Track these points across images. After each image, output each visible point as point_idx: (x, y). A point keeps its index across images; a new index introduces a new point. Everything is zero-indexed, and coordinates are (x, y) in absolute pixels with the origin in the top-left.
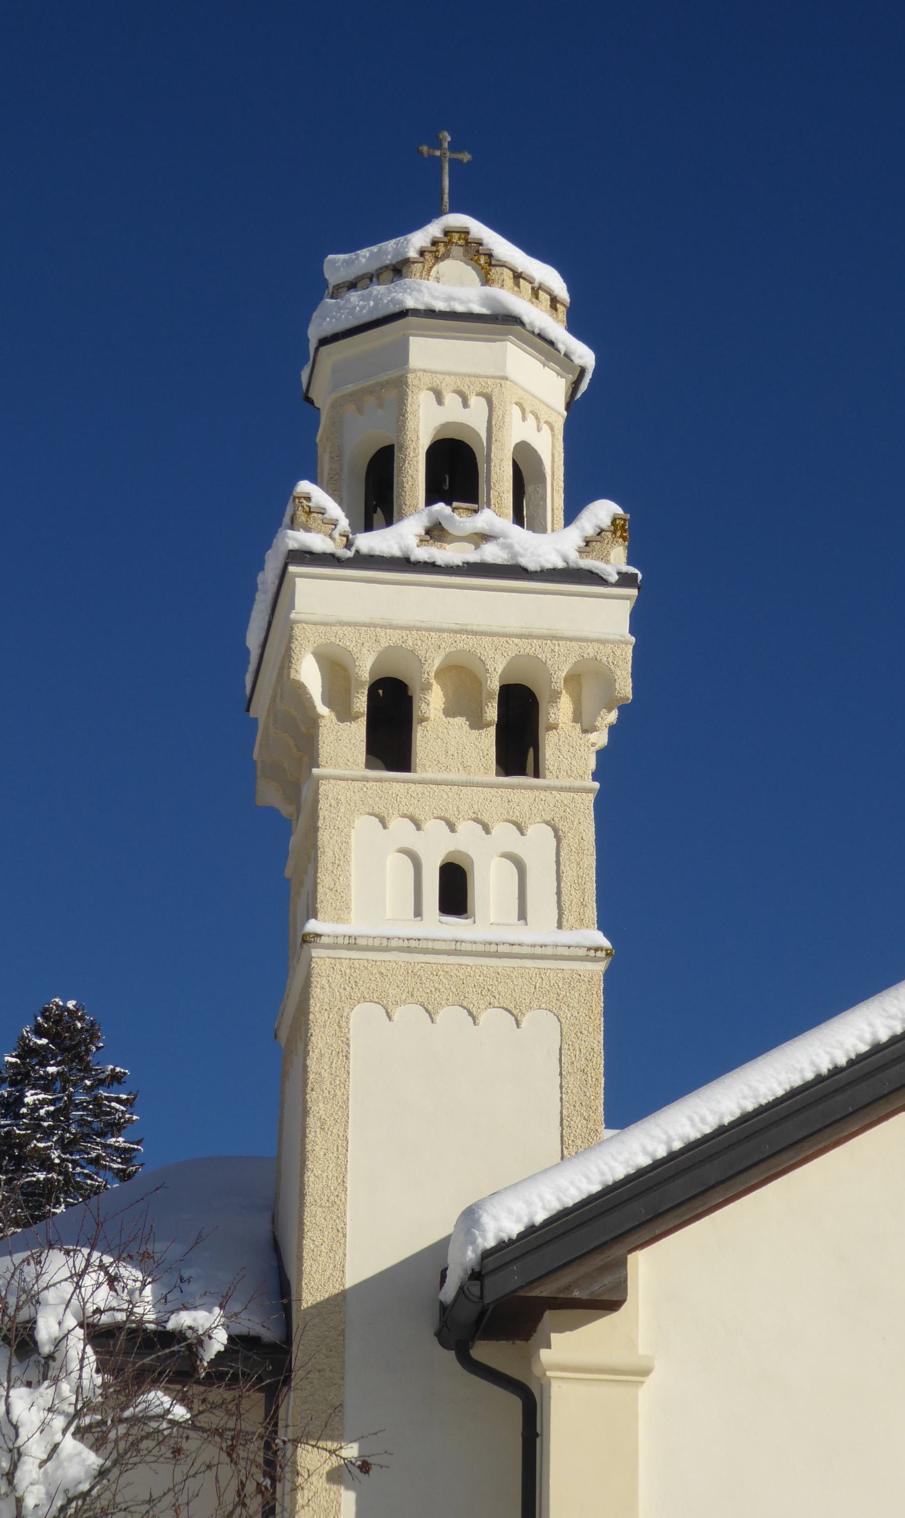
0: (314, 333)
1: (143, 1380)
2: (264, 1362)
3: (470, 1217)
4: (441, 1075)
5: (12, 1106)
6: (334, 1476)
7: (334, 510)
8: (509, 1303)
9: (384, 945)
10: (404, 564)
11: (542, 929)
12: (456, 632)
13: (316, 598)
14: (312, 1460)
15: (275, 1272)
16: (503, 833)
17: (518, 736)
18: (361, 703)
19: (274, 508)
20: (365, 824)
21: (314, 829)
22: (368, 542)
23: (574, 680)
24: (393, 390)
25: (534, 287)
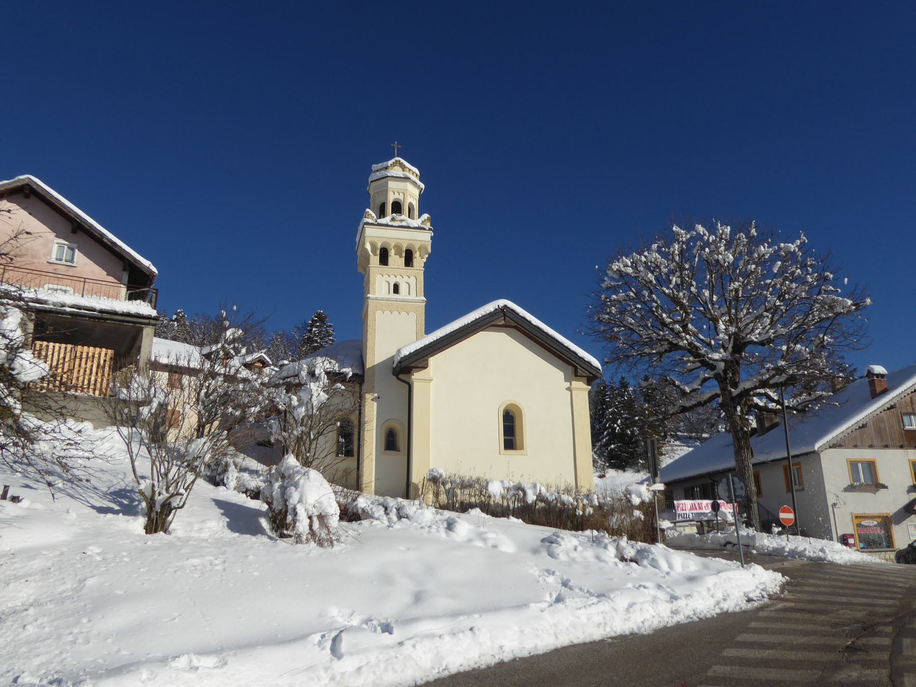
0: (370, 180)
1: (335, 382)
2: (359, 378)
3: (399, 351)
4: (393, 323)
5: (310, 331)
6: (373, 400)
7: (373, 215)
8: (406, 368)
9: (383, 299)
10: (387, 225)
11: (413, 296)
12: (360, 410)
13: (370, 232)
14: (369, 397)
15: (361, 361)
16: (406, 278)
17: (409, 261)
18: (378, 252)
19: (362, 214)
20: (379, 276)
21: (369, 277)
22: (380, 221)
23: (419, 249)
24: (385, 192)
25: (413, 172)
